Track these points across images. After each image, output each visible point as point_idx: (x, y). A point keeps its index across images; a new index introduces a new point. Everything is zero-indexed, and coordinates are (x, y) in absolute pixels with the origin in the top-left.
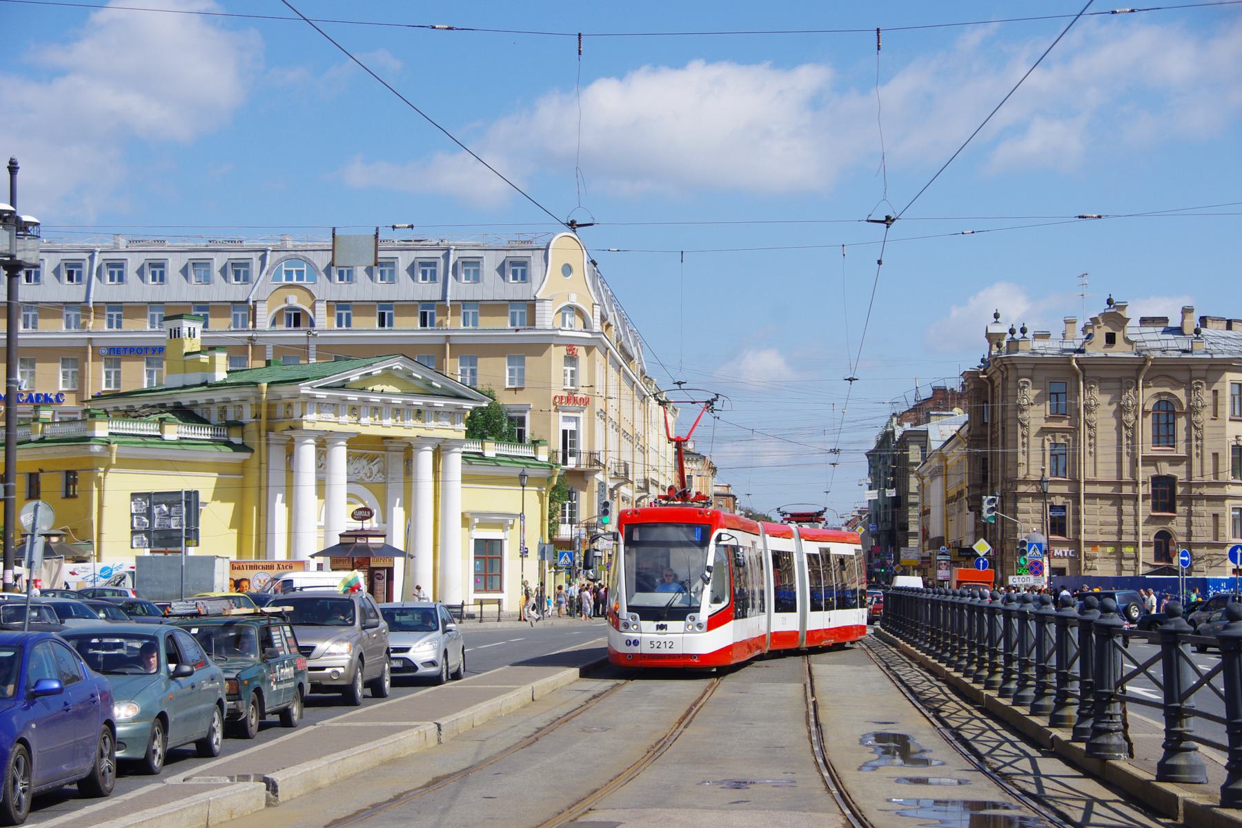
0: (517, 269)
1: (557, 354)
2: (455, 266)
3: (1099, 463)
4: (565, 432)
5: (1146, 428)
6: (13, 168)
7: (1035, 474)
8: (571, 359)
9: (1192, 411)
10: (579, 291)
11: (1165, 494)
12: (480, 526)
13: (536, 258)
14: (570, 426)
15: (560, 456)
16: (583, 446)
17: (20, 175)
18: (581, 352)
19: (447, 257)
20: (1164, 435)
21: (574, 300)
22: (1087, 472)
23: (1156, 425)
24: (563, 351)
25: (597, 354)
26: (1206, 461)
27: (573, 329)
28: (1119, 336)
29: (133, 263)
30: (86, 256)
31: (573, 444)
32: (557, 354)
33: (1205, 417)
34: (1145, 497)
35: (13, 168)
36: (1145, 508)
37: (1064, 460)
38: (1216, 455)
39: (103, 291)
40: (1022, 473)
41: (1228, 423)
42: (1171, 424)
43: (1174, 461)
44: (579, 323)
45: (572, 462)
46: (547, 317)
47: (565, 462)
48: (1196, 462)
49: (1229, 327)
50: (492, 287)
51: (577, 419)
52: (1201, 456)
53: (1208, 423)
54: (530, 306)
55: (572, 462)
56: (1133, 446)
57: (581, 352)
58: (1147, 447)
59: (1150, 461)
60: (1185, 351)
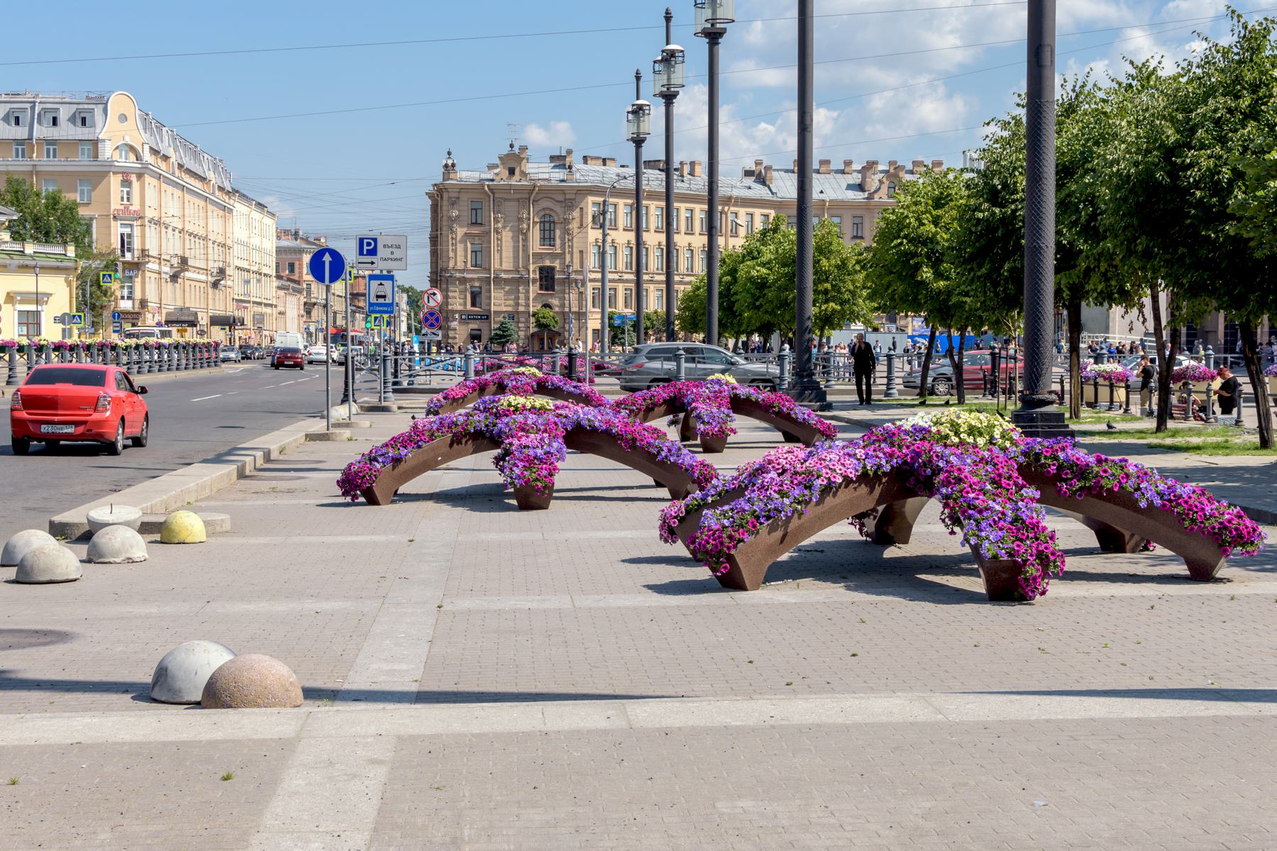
0: (83, 121)
1: (115, 181)
2: (39, 115)
3: (503, 258)
4: (122, 236)
5: (535, 234)
6: (668, 18)
7: (460, 265)
8: (126, 183)
9: (566, 221)
10: (135, 134)
11: (547, 279)
12: (21, 302)
13: (98, 110)
14: (128, 230)
15: (119, 252)
16: (137, 244)
17: (672, 23)
18: (133, 178)
19: (33, 108)
20: (548, 238)
21: (128, 140)
22: (495, 264)
23: (543, 230)
24: (120, 177)
25: (147, 179)
26: (504, 254)
27: (130, 162)
28: (517, 171)
29: (64, 114)
30: (28, 106)
31: (129, 243)
32: (115, 181)
33: (574, 226)
34: (534, 281)
35: (668, 18)
36: (534, 289)
37: (480, 257)
38: (581, 252)
39: (41, 131)
40: (451, 264)
41: (590, 231)
42: (552, 231)
43: (553, 256)
44: (132, 157)
45: (128, 257)
46: (107, 151)
47: (123, 256)
48: (568, 257)
49: (604, 164)
50: (67, 131)
51: (131, 226)
52: (571, 253)
53: (576, 231)
54: (95, 143)
55: (128, 257)
56: (526, 247)
57: (133, 178)
58: (535, 245)
59: (539, 256)
60: (563, 181)
